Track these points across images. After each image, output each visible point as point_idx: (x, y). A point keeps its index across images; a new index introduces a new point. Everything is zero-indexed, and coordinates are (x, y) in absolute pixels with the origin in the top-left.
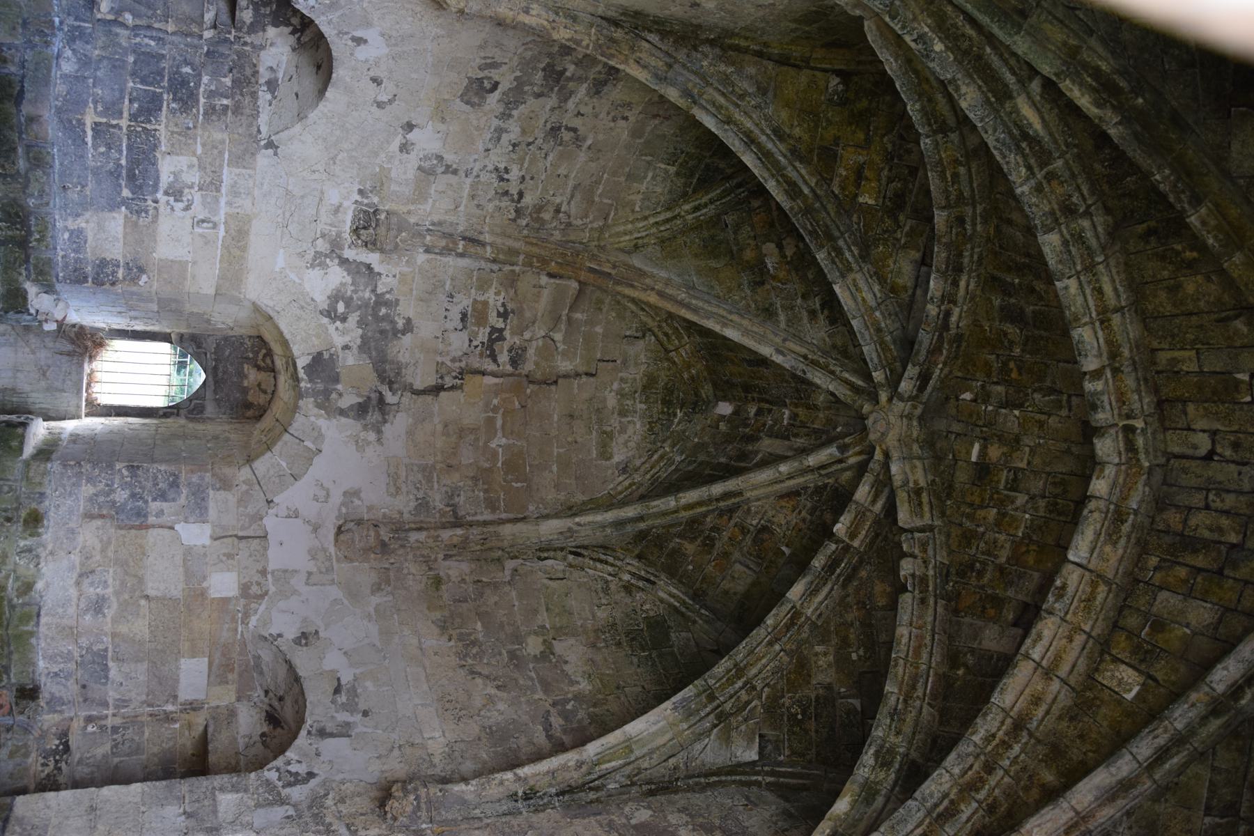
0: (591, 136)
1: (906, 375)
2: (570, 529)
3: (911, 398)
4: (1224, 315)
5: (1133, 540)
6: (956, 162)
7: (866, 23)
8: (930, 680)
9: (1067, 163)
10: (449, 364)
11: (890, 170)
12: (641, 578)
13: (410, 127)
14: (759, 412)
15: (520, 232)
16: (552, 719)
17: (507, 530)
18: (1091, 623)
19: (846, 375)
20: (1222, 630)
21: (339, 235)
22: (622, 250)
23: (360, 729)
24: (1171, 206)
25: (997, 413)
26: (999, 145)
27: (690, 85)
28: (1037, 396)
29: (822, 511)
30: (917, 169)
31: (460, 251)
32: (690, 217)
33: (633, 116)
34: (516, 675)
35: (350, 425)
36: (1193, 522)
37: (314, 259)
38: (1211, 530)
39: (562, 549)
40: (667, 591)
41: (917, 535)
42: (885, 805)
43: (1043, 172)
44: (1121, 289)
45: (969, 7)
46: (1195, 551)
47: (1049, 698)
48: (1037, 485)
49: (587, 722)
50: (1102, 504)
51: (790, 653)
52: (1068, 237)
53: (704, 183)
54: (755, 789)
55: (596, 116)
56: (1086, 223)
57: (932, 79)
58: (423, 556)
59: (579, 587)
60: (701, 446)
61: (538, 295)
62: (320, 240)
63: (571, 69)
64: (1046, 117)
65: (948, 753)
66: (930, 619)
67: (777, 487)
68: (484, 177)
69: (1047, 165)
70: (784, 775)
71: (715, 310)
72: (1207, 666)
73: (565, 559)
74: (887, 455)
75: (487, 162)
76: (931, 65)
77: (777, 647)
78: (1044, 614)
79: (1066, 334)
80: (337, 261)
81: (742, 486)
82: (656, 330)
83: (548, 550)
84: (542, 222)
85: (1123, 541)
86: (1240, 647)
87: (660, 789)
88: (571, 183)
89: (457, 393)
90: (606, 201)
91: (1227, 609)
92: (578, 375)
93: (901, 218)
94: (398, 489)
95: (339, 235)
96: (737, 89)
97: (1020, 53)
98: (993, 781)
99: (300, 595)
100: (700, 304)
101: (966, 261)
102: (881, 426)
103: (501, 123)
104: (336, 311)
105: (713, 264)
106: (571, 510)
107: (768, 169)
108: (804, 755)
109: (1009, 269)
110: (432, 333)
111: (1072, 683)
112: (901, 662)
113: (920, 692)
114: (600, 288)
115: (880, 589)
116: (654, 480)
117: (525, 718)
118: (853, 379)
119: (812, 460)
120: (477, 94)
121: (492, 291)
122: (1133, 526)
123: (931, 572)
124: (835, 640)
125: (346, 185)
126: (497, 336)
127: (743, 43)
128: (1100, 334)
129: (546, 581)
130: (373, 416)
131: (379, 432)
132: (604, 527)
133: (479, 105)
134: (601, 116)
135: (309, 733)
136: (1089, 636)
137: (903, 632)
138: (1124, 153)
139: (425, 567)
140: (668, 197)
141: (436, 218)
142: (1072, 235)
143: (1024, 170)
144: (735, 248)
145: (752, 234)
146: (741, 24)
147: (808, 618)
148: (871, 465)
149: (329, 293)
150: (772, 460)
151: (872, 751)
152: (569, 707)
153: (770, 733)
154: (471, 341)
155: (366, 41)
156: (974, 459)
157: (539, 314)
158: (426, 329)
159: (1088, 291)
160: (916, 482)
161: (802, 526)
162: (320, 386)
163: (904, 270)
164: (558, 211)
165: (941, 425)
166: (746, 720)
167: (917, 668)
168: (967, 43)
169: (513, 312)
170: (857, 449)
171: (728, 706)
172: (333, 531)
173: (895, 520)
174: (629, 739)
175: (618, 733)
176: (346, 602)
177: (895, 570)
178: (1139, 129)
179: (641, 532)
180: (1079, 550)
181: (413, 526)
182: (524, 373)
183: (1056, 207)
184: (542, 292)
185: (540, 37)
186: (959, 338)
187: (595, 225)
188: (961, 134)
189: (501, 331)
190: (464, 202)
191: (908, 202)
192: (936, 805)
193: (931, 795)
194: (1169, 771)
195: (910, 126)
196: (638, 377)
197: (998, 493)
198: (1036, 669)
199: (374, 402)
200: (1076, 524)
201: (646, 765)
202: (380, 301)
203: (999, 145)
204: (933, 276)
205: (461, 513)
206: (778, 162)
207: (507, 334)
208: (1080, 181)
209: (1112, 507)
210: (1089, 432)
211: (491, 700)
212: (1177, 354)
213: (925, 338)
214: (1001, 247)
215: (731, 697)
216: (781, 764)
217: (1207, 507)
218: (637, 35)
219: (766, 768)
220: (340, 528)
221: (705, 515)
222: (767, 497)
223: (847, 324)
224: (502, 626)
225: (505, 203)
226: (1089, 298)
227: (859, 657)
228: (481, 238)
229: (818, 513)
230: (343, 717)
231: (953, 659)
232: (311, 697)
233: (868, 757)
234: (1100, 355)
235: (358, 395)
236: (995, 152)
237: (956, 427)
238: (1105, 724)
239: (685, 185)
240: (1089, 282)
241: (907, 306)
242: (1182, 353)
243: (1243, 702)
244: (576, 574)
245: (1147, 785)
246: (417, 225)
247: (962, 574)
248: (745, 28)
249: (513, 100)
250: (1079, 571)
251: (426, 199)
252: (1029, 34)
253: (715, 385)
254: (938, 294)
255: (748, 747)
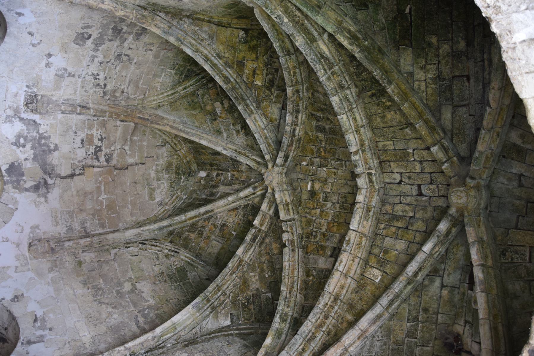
0: (136, 58)
1: (279, 156)
2: (139, 233)
3: (281, 166)
4: (402, 127)
5: (374, 218)
6: (295, 67)
7: (255, 10)
8: (299, 283)
9: (339, 67)
10: (77, 163)
11: (267, 70)
12: (172, 251)
13: (49, 55)
14: (218, 175)
15: (106, 102)
16: (139, 319)
17: (110, 236)
18: (361, 253)
19: (254, 157)
20: (409, 251)
21: (18, 107)
22: (153, 108)
23: (49, 337)
24: (380, 84)
25: (317, 170)
26: (312, 61)
27: (179, 36)
28: (333, 162)
29: (248, 215)
30: (278, 70)
31: (78, 112)
32: (182, 92)
33: (154, 49)
34: (121, 301)
35: (32, 195)
36: (396, 209)
37: (6, 119)
38: (403, 212)
39: (136, 242)
40: (185, 255)
41: (288, 223)
42: (286, 338)
43: (330, 72)
44: (363, 118)
45: (298, 4)
46: (397, 220)
47: (347, 286)
48: (335, 198)
49: (154, 318)
50: (361, 205)
51: (240, 278)
52: (342, 98)
53: (188, 77)
54: (231, 337)
55: (138, 49)
56: (348, 92)
57: (283, 33)
58: (72, 252)
59: (145, 258)
60: (194, 191)
61: (116, 130)
62: (8, 109)
63: (125, 29)
64: (331, 49)
65: (309, 313)
66: (297, 257)
67: (228, 207)
68: (87, 78)
69: (332, 68)
70: (242, 329)
71: (195, 132)
72: (405, 266)
73: (138, 246)
74: (273, 190)
75: (88, 71)
76: (283, 28)
77: (234, 276)
78: (342, 252)
79: (343, 136)
80: (18, 119)
81: (213, 208)
82: (170, 142)
83: (130, 243)
84: (116, 97)
85: (370, 219)
86: (416, 257)
87: (190, 343)
88: (128, 79)
89: (82, 177)
90: (144, 87)
91: (411, 242)
92: (137, 164)
93: (273, 90)
94: (57, 223)
95: (18, 107)
96: (200, 37)
97: (319, 23)
98: (328, 322)
99: (12, 278)
100: (189, 130)
101: (301, 108)
102: (270, 178)
103: (94, 53)
104: (19, 143)
105: (194, 112)
106: (139, 225)
107: (215, 71)
108: (250, 320)
109: (318, 111)
110: (68, 150)
111: (355, 278)
112: (287, 277)
113: (295, 289)
114: (144, 125)
115: (275, 246)
116: (174, 207)
117: (127, 320)
118: (257, 159)
119: (242, 194)
120: (81, 40)
121: (95, 129)
122: (374, 212)
123: (295, 238)
124: (258, 270)
125: (20, 83)
126: (98, 149)
127: (202, 17)
128: (356, 136)
129: (130, 257)
130: (43, 190)
131: (46, 197)
132: (154, 231)
133: (83, 45)
134: (140, 49)
135: (22, 343)
136: (361, 259)
137: (286, 264)
138: (361, 63)
139: (73, 257)
140: (172, 84)
141: (66, 97)
142: (343, 97)
143: (323, 71)
144: (202, 105)
145: (210, 99)
146: (201, 9)
147: (246, 262)
148: (267, 195)
149: (15, 134)
150: (226, 195)
151: (278, 316)
152: (146, 312)
153: (234, 312)
154: (86, 152)
155: (23, 15)
156: (309, 189)
157: (117, 138)
158: (65, 148)
159: (351, 120)
160: (286, 201)
161: (240, 222)
162: (14, 178)
163: (275, 112)
164: (123, 92)
165: (294, 176)
166: (224, 308)
167: (293, 278)
168: (297, 19)
169: (105, 138)
170: (261, 188)
171: (216, 304)
172: (27, 246)
173: (279, 217)
174: (174, 324)
175: (169, 322)
176: (36, 278)
177: (280, 238)
178: (367, 54)
179: (171, 231)
180: (354, 224)
181: (66, 239)
182: (112, 165)
183: (336, 85)
184: (118, 129)
185: (110, 15)
186: (299, 140)
187: (140, 97)
188: (296, 56)
189: (100, 147)
190: (79, 89)
191: (276, 83)
192: (307, 336)
193: (304, 332)
194: (394, 308)
195: (275, 52)
196: (164, 163)
197: (320, 202)
198: (341, 275)
199: (42, 184)
200: (352, 213)
201: (183, 334)
202: (42, 137)
203: (312, 61)
204: (287, 115)
205: (88, 231)
206: (219, 68)
207: (103, 148)
208: (345, 75)
209: (365, 206)
210: (354, 176)
211: (110, 314)
212: (385, 143)
213: (286, 141)
214: (314, 102)
215: (217, 299)
216: (240, 325)
217: (401, 203)
218: (154, 13)
219: (234, 328)
220: (30, 244)
221: (198, 221)
222: (224, 211)
223: (253, 135)
224: (112, 279)
225: (98, 89)
226: (351, 122)
227: (269, 276)
228: (88, 106)
229: (246, 216)
230: (40, 333)
231: (307, 273)
232: (22, 326)
233: (277, 319)
234: (357, 145)
235: (34, 181)
236: (311, 64)
237: (301, 176)
238: (369, 293)
239: (179, 78)
240: (351, 116)
241: (278, 127)
242: (388, 142)
243: (418, 278)
244: (143, 252)
245: (387, 315)
246: (57, 101)
247: (308, 237)
248: (202, 11)
249: (99, 42)
250: (355, 233)
251: (60, 89)
252: (322, 15)
253: (198, 165)
254: (290, 122)
255: (226, 319)
